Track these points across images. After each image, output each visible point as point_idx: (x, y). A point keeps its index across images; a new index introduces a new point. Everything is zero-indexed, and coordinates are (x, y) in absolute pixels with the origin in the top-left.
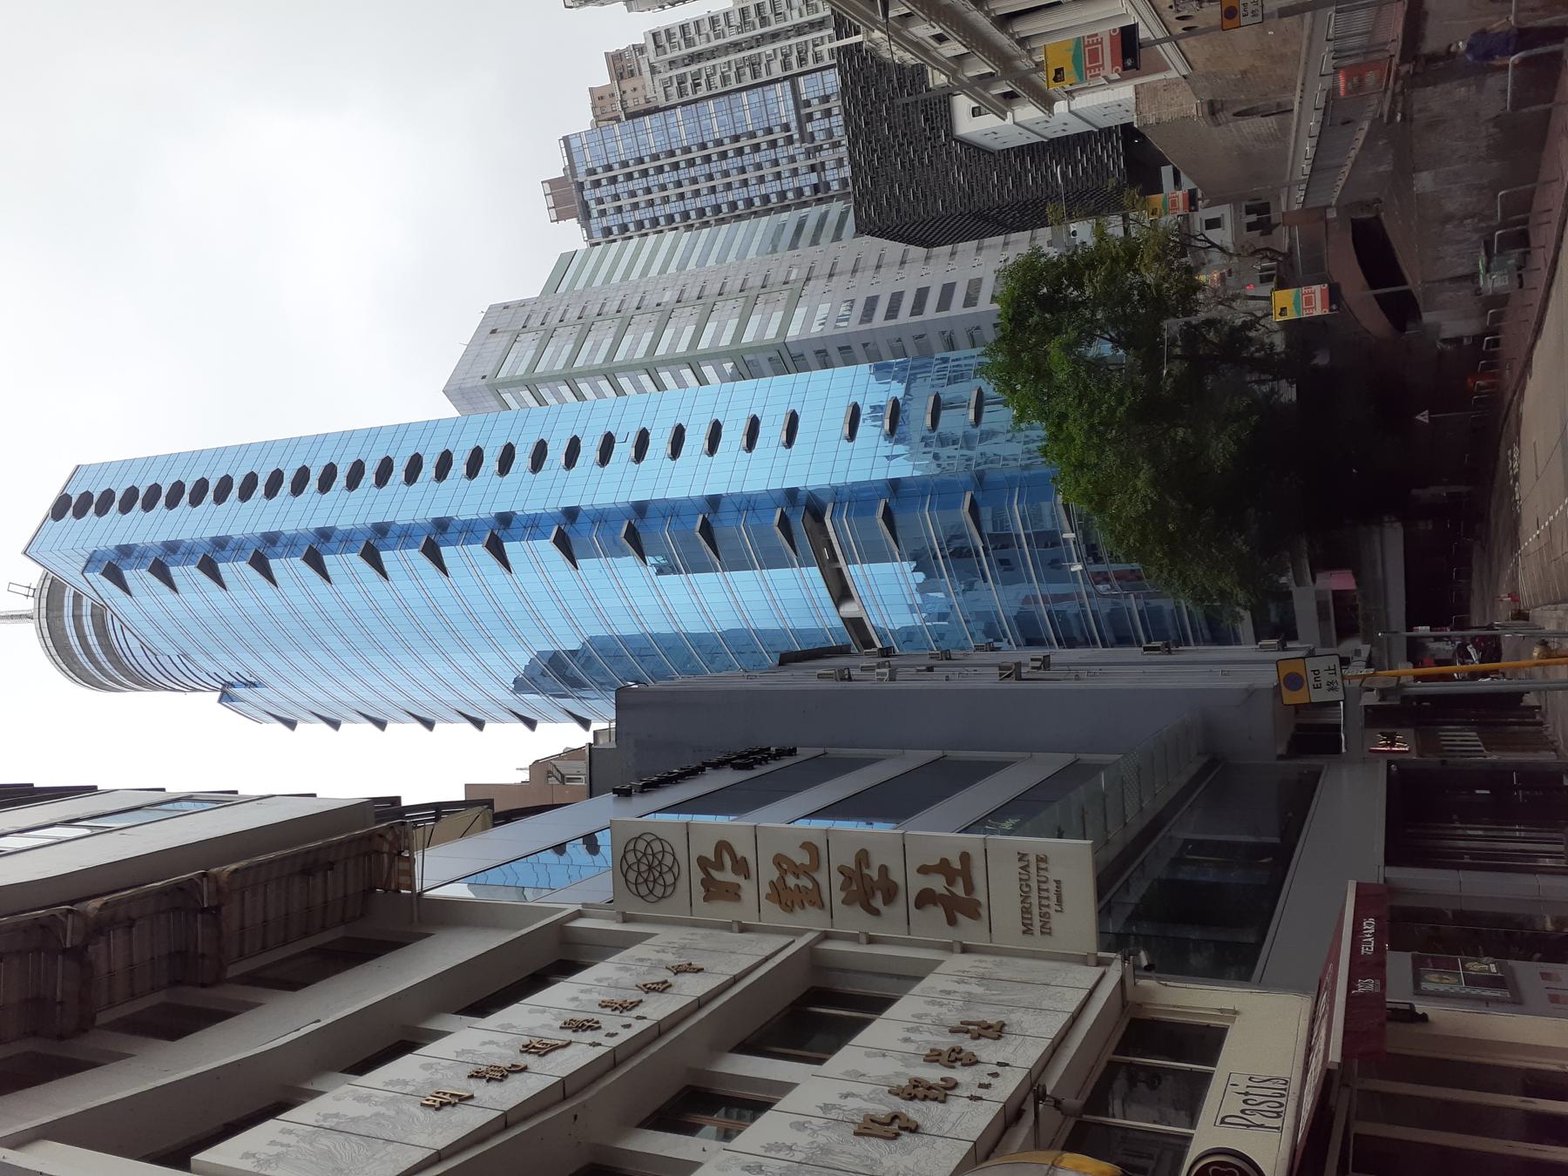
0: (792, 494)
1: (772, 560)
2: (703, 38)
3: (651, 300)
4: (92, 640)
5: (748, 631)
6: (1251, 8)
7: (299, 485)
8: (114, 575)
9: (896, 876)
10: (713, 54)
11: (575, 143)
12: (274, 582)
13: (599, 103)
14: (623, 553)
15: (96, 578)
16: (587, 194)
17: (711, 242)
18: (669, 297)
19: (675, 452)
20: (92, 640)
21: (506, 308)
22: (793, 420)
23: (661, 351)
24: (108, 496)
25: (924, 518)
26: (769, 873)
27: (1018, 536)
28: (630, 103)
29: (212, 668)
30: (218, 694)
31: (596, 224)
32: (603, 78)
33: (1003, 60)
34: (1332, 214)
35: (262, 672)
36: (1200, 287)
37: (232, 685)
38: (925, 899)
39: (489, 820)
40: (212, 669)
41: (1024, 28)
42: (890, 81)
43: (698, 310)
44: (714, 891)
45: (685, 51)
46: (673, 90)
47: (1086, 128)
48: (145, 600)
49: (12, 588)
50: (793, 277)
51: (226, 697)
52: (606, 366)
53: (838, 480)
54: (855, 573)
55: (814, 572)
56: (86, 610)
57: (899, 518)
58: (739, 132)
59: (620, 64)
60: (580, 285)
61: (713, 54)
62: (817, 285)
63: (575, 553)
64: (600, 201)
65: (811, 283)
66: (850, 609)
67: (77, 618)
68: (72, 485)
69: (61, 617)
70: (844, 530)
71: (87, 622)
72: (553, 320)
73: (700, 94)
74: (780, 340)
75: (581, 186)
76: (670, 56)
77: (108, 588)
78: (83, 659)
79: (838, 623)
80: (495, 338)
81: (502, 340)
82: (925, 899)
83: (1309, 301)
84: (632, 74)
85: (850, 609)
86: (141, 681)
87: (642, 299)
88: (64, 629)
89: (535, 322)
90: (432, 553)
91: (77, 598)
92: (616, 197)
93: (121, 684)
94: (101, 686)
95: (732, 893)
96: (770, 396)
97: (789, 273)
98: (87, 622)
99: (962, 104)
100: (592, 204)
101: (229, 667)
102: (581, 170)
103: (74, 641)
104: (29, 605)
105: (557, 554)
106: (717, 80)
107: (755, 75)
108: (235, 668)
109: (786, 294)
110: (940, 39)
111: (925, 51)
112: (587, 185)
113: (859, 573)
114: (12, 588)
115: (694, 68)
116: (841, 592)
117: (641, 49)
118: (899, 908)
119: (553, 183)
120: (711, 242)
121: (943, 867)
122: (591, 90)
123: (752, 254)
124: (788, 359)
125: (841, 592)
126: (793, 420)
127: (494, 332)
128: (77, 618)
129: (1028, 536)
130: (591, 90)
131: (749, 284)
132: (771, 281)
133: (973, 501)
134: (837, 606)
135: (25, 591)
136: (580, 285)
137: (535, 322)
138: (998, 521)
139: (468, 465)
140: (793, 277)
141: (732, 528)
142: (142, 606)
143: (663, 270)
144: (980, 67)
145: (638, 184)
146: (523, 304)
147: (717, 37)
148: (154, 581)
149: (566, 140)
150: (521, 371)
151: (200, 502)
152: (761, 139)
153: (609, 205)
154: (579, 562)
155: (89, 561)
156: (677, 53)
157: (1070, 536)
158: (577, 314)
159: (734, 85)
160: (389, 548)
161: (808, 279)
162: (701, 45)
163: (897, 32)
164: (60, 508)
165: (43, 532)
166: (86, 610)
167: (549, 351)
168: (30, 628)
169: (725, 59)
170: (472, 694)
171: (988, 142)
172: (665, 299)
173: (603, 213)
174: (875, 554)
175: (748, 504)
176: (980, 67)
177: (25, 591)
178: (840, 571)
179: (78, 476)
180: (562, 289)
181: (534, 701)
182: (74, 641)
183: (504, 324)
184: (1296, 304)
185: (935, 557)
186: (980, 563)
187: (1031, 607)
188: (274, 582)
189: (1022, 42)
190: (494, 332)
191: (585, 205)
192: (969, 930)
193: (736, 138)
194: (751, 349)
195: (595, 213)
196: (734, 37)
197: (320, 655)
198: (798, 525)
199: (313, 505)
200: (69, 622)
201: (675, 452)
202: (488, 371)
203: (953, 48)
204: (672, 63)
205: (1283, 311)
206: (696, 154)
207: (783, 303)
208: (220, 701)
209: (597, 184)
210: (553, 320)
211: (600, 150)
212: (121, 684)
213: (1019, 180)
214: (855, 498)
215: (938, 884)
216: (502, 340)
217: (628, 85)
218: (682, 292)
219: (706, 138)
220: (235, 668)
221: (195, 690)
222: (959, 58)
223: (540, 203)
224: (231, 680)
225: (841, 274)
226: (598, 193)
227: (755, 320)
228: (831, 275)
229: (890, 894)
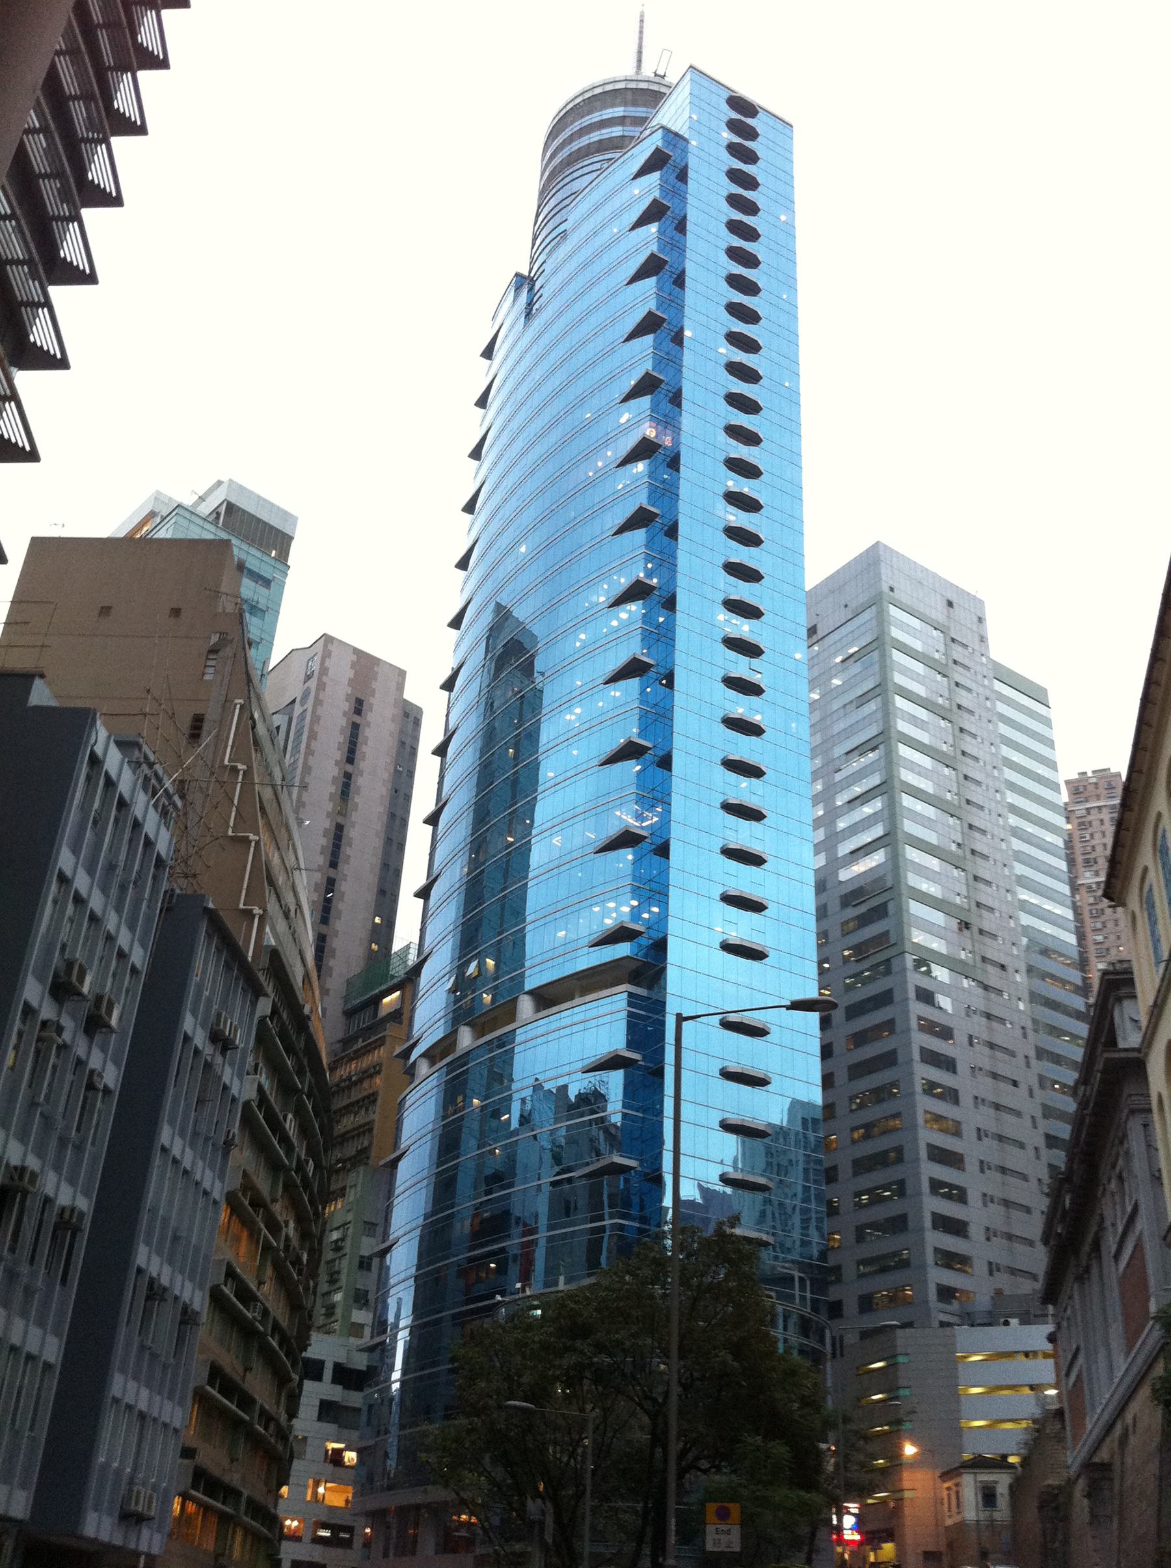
4: (595, 136)
5: (524, 921)
7: (738, 370)
8: (657, 162)
15: (655, 141)
17: (1049, 871)
19: (730, 808)
20: (595, 136)
21: (980, 620)
22: (756, 955)
23: (907, 801)
24: (750, 157)
35: (537, 323)
37: (531, 290)
39: (279, 566)
40: (548, 267)
49: (666, 54)
51: (522, 282)
60: (1001, 708)
62: (978, 999)
65: (980, 991)
67: (621, 121)
68: (771, 121)
72: (958, 675)
74: (908, 947)
77: (641, 154)
78: (576, 126)
80: (941, 605)
81: (938, 613)
86: (544, 193)
87: (978, 783)
88: (613, 106)
89: (958, 653)
90: (640, 519)
101: (548, 288)
103: (596, 117)
104: (647, 72)
108: (546, 293)
114: (666, 54)
120: (1049, 871)
123: (1026, 919)
126: (756, 955)
127: (950, 604)
128: (621, 121)
133: (628, 1169)
136: (1001, 708)
137: (958, 653)
139: (740, 564)
142: (625, 188)
146: (983, 639)
150: (899, 679)
151: (730, 257)
155: (676, 134)
158: (964, 703)
161: (986, 988)
164: (740, 104)
165: (714, 87)
167: (919, 668)
168: (628, 70)
179: (779, 126)
180: (998, 686)
181: (478, 624)
187: (516, 1231)
190: (950, 604)
194: (901, 910)
199: (711, 386)
201: (730, 808)
208: (517, 275)
210: (958, 675)
216: (938, 613)
224: (538, 285)
225: (991, 1029)
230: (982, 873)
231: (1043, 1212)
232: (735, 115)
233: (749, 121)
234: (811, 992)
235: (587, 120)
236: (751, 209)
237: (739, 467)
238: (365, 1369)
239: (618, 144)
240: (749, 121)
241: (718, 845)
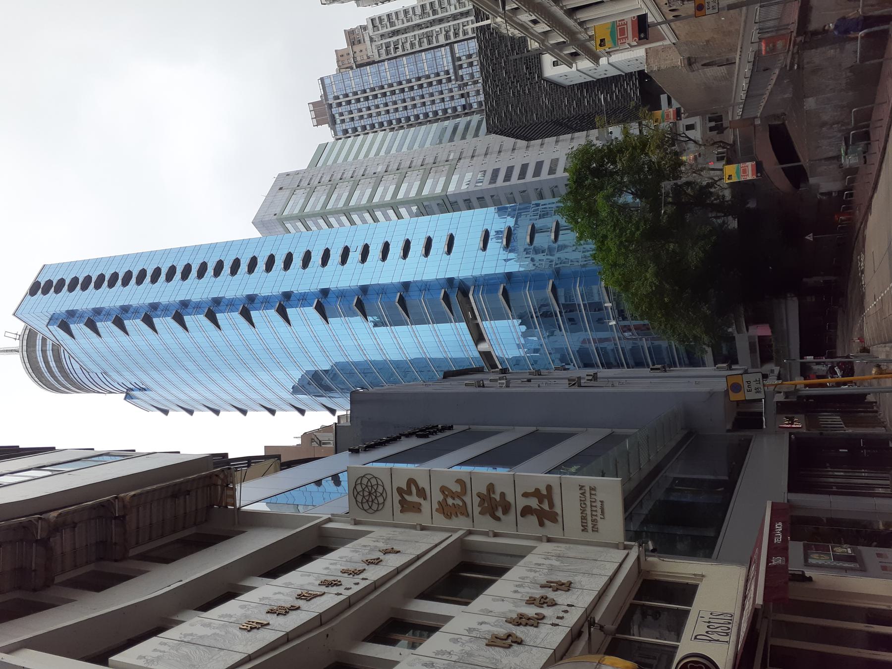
0: (450, 281)
1: (439, 319)
2: (400, 22)
3: (370, 171)
4: (53, 364)
6: (711, 4)
7: (170, 276)
8: (65, 327)
9: (510, 498)
10: (405, 30)
11: (327, 82)
12: (156, 331)
13: (341, 59)
14: (354, 315)
15: (55, 329)
16: (334, 111)
17: (404, 138)
18: (380, 169)
19: (384, 257)
20: (53, 364)
21: (288, 175)
22: (451, 239)
23: (376, 200)
24: (61, 282)
25: (525, 295)
26: (438, 497)
27: (579, 305)
28: (359, 59)
29: (121, 380)
30: (124, 395)
31: (339, 127)
32: (343, 45)
33: (571, 34)
35: (149, 383)
36: (682, 163)
37: (132, 390)
38: (526, 511)
39: (278, 466)
40: (121, 380)
41: (583, 16)
43: (397, 176)
44: (406, 507)
45: (390, 29)
46: (383, 51)
47: (618, 73)
48: (82, 341)
49: (7, 334)
50: (451, 158)
51: (128, 397)
52: (345, 208)
53: (477, 273)
54: (487, 326)
55: (463, 325)
56: (49, 347)
57: (512, 295)
58: (421, 75)
59: (353, 37)
60: (330, 162)
61: (405, 30)
62: (465, 162)
63: (327, 315)
64: (341, 114)
65: (462, 161)
66: (483, 347)
67: (44, 351)
68: (41, 276)
69: (35, 351)
70: (480, 301)
71: (50, 354)
72: (315, 182)
73: (398, 54)
74: (444, 194)
75: (330, 106)
76: (381, 32)
77: (61, 334)
78: (47, 375)
79: (477, 355)
80: (282, 193)
81: (286, 193)
82: (526, 511)
84: (359, 42)
85: (483, 347)
86: (80, 387)
87: (365, 170)
88: (36, 358)
89: (304, 183)
90: (246, 314)
91: (44, 340)
92: (351, 112)
94: (58, 390)
95: (417, 508)
96: (438, 226)
97: (449, 155)
98: (50, 354)
99: (547, 59)
100: (337, 116)
101: (130, 379)
102: (330, 97)
103: (42, 365)
104: (16, 344)
105: (317, 315)
106: (408, 45)
107: (429, 43)
108: (134, 380)
109: (447, 167)
110: (535, 22)
111: (526, 29)
112: (334, 105)
113: (489, 326)
114: (7, 334)
115: (395, 39)
116: (479, 337)
117: (365, 28)
118: (511, 516)
119: (315, 104)
120: (404, 138)
121: (537, 493)
122: (336, 51)
123: (428, 144)
124: (448, 204)
125: (479, 337)
126: (451, 239)
127: (281, 189)
128: (44, 351)
129: (585, 305)
130: (336, 51)
131: (426, 162)
132: (438, 160)
133: (553, 285)
134: (476, 345)
135: (14, 336)
136: (330, 162)
137: (304, 183)
138: (568, 296)
139: (266, 265)
140: (451, 158)
141: (416, 300)
142: (81, 345)
143: (377, 154)
144: (557, 38)
145: (363, 105)
146: (297, 173)
147: (408, 21)
148: (88, 331)
149: (322, 79)
151: (114, 286)
152: (433, 79)
153: (346, 117)
154: (329, 320)
155: (50, 319)
156: (385, 30)
157: (609, 305)
158: (328, 179)
159: (417, 48)
160: (221, 312)
161: (460, 159)
162: (399, 26)
163: (511, 18)
164: (34, 289)
165: (25, 303)
166: (49, 347)
167: (312, 200)
168: (17, 357)
169: (413, 34)
170: (269, 395)
172: (379, 170)
173: (343, 121)
174: (498, 315)
175: (426, 287)
176: (557, 38)
177: (14, 336)
178: (478, 325)
179: (45, 271)
180: (319, 165)
181: (304, 399)
182: (42, 365)
183: (287, 184)
188: (156, 331)
189: (581, 24)
190: (281, 189)
191: (333, 117)
192: (551, 529)
193: (419, 79)
194: (427, 199)
195: (338, 121)
196: (417, 21)
197: (182, 373)
198: (454, 299)
199: (178, 288)
200: (39, 354)
201: (384, 257)
202: (278, 211)
203: (542, 27)
204: (382, 36)
206: (396, 87)
207: (445, 172)
208: (125, 399)
209: (340, 105)
210: (315, 182)
211: (341, 86)
213: (579, 103)
214: (487, 284)
215: (533, 503)
216: (286, 193)
217: (357, 48)
218: (388, 166)
219: (402, 79)
220: (134, 380)
221: (111, 392)
222: (545, 33)
223: (307, 116)
224: (132, 387)
225: (478, 156)
226: (340, 110)
227: (429, 182)
228: (473, 157)
229: (507, 508)
231: (557, 142)
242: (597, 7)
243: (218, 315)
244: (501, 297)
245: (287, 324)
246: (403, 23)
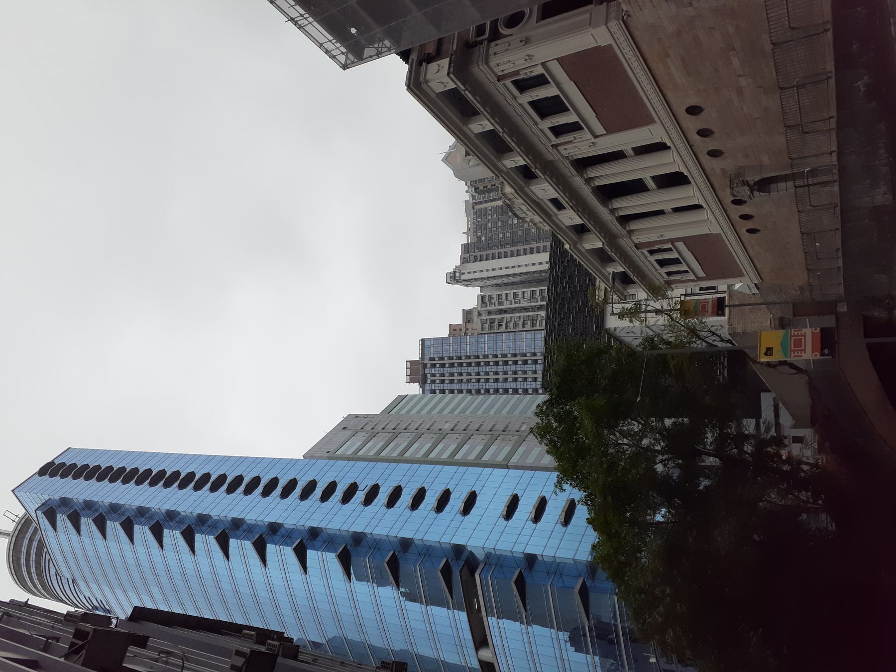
0: (458, 550)
1: (434, 600)
2: (508, 302)
3: (436, 427)
4: (33, 557)
10: (513, 310)
11: (427, 343)
13: (453, 332)
16: (427, 371)
17: (482, 403)
18: (447, 427)
25: (415, 569)
31: (428, 387)
34: (843, 308)
40: (88, 594)
42: (577, 302)
43: (462, 436)
45: (497, 307)
46: (487, 326)
49: (7, 514)
50: (523, 429)
53: (490, 545)
54: (493, 624)
55: (463, 616)
56: (37, 538)
58: (517, 352)
61: (513, 310)
64: (433, 375)
66: (485, 654)
67: (31, 541)
69: (23, 538)
70: (488, 587)
73: (501, 330)
75: (425, 366)
76: (489, 308)
79: (476, 665)
81: (348, 433)
83: (798, 343)
85: (485, 654)
89: (368, 428)
92: (443, 375)
93: (36, 587)
97: (521, 426)
100: (429, 376)
102: (427, 357)
106: (511, 325)
107: (533, 325)
109: (516, 437)
112: (429, 366)
113: (495, 625)
114: (7, 514)
115: (500, 316)
116: (481, 640)
119: (412, 363)
120: (482, 403)
125: (481, 640)
127: (344, 428)
128: (31, 541)
131: (496, 428)
134: (477, 649)
135: (13, 517)
136: (403, 412)
137: (368, 428)
140: (523, 429)
141: (412, 567)
143: (452, 412)
145: (456, 370)
147: (516, 303)
148: (94, 528)
149: (423, 340)
152: (529, 357)
153: (438, 378)
156: (493, 307)
159: (520, 328)
162: (506, 306)
164: (42, 472)
169: (518, 315)
171: (621, 335)
172: (445, 427)
173: (433, 382)
175: (428, 552)
177: (13, 517)
183: (353, 425)
184: (783, 345)
185: (585, 636)
186: (620, 650)
190: (344, 428)
191: (425, 376)
193: (515, 355)
195: (429, 381)
196: (524, 304)
200: (26, 542)
202: (332, 449)
204: (490, 313)
205: (769, 351)
206: (491, 359)
207: (512, 442)
209: (434, 366)
211: (439, 349)
212: (36, 587)
216: (348, 433)
218: (456, 425)
219: (498, 353)
220: (100, 597)
223: (402, 372)
224: (96, 604)
226: (433, 371)
227: (493, 448)
230: (476, 427)
232: (229, 480)
233: (197, 478)
234: (603, 27)
235: (23, 556)
236: (239, 480)
237: (374, 491)
238: (445, 333)
239: (41, 545)
240: (197, 478)
241: (502, 522)
242: (693, 211)
243: (83, 519)
244: (577, 598)
245: (346, 578)
246: (506, 295)
